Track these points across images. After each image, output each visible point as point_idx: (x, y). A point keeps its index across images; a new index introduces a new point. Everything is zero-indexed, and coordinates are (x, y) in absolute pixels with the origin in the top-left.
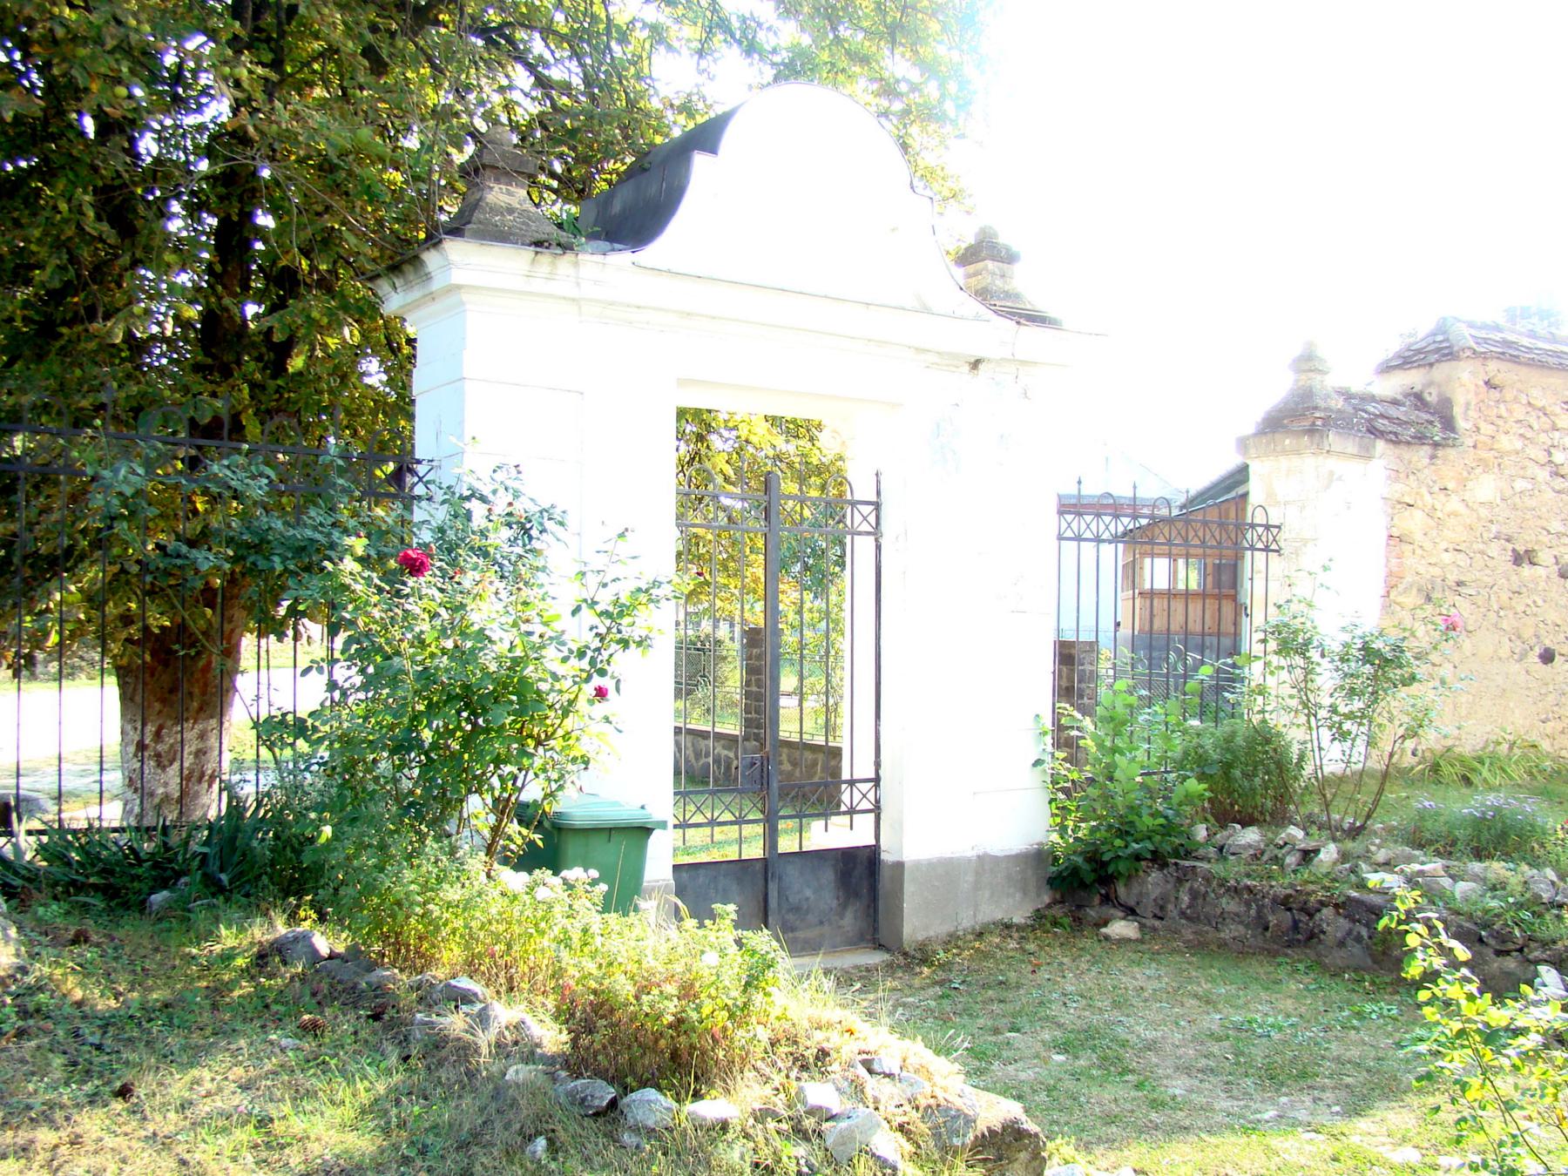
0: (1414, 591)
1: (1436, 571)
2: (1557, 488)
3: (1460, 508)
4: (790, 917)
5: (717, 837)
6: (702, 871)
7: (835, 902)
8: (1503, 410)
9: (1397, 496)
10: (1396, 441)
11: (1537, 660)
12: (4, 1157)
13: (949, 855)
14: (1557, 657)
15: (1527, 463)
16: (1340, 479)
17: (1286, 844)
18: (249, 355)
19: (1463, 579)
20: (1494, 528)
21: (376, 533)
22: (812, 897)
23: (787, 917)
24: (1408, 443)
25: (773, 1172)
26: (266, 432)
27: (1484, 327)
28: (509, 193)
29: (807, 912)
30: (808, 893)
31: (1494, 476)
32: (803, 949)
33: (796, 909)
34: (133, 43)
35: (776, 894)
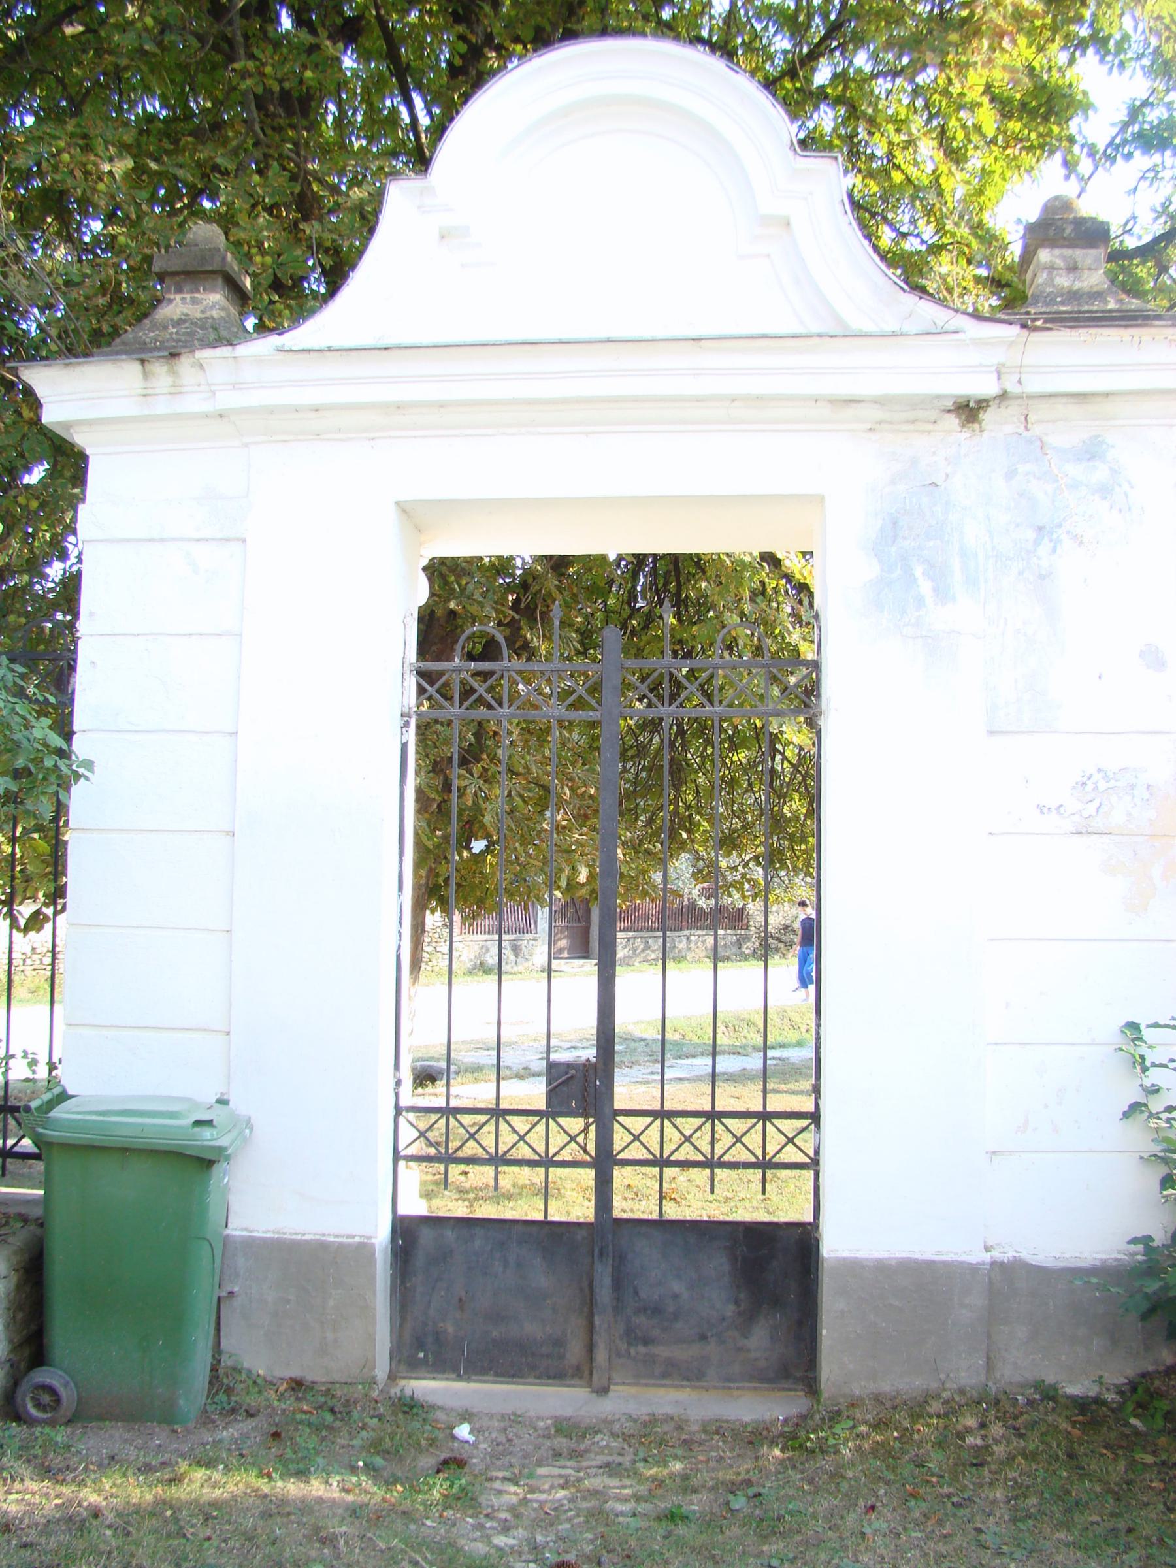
4: (641, 1320)
5: (505, 1183)
6: (479, 1231)
7: (730, 1310)
13: (929, 1256)
18: (736, 37)
22: (685, 1295)
23: (636, 1320)
28: (194, 301)
29: (676, 1316)
30: (677, 1287)
32: (665, 1375)
33: (656, 1310)
35: (607, 1281)
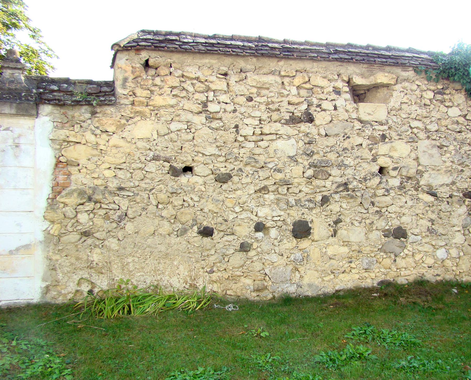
0: (75, 195)
1: (99, 182)
2: (447, 105)
3: (121, 143)
9: (62, 137)
10: (59, 104)
11: (196, 234)
12: (0, 314)
14: (216, 232)
15: (180, 112)
19: (123, 186)
20: (151, 154)
24: (70, 105)
25: (176, 378)
26: (235, 72)
27: (209, 37)
31: (151, 122)
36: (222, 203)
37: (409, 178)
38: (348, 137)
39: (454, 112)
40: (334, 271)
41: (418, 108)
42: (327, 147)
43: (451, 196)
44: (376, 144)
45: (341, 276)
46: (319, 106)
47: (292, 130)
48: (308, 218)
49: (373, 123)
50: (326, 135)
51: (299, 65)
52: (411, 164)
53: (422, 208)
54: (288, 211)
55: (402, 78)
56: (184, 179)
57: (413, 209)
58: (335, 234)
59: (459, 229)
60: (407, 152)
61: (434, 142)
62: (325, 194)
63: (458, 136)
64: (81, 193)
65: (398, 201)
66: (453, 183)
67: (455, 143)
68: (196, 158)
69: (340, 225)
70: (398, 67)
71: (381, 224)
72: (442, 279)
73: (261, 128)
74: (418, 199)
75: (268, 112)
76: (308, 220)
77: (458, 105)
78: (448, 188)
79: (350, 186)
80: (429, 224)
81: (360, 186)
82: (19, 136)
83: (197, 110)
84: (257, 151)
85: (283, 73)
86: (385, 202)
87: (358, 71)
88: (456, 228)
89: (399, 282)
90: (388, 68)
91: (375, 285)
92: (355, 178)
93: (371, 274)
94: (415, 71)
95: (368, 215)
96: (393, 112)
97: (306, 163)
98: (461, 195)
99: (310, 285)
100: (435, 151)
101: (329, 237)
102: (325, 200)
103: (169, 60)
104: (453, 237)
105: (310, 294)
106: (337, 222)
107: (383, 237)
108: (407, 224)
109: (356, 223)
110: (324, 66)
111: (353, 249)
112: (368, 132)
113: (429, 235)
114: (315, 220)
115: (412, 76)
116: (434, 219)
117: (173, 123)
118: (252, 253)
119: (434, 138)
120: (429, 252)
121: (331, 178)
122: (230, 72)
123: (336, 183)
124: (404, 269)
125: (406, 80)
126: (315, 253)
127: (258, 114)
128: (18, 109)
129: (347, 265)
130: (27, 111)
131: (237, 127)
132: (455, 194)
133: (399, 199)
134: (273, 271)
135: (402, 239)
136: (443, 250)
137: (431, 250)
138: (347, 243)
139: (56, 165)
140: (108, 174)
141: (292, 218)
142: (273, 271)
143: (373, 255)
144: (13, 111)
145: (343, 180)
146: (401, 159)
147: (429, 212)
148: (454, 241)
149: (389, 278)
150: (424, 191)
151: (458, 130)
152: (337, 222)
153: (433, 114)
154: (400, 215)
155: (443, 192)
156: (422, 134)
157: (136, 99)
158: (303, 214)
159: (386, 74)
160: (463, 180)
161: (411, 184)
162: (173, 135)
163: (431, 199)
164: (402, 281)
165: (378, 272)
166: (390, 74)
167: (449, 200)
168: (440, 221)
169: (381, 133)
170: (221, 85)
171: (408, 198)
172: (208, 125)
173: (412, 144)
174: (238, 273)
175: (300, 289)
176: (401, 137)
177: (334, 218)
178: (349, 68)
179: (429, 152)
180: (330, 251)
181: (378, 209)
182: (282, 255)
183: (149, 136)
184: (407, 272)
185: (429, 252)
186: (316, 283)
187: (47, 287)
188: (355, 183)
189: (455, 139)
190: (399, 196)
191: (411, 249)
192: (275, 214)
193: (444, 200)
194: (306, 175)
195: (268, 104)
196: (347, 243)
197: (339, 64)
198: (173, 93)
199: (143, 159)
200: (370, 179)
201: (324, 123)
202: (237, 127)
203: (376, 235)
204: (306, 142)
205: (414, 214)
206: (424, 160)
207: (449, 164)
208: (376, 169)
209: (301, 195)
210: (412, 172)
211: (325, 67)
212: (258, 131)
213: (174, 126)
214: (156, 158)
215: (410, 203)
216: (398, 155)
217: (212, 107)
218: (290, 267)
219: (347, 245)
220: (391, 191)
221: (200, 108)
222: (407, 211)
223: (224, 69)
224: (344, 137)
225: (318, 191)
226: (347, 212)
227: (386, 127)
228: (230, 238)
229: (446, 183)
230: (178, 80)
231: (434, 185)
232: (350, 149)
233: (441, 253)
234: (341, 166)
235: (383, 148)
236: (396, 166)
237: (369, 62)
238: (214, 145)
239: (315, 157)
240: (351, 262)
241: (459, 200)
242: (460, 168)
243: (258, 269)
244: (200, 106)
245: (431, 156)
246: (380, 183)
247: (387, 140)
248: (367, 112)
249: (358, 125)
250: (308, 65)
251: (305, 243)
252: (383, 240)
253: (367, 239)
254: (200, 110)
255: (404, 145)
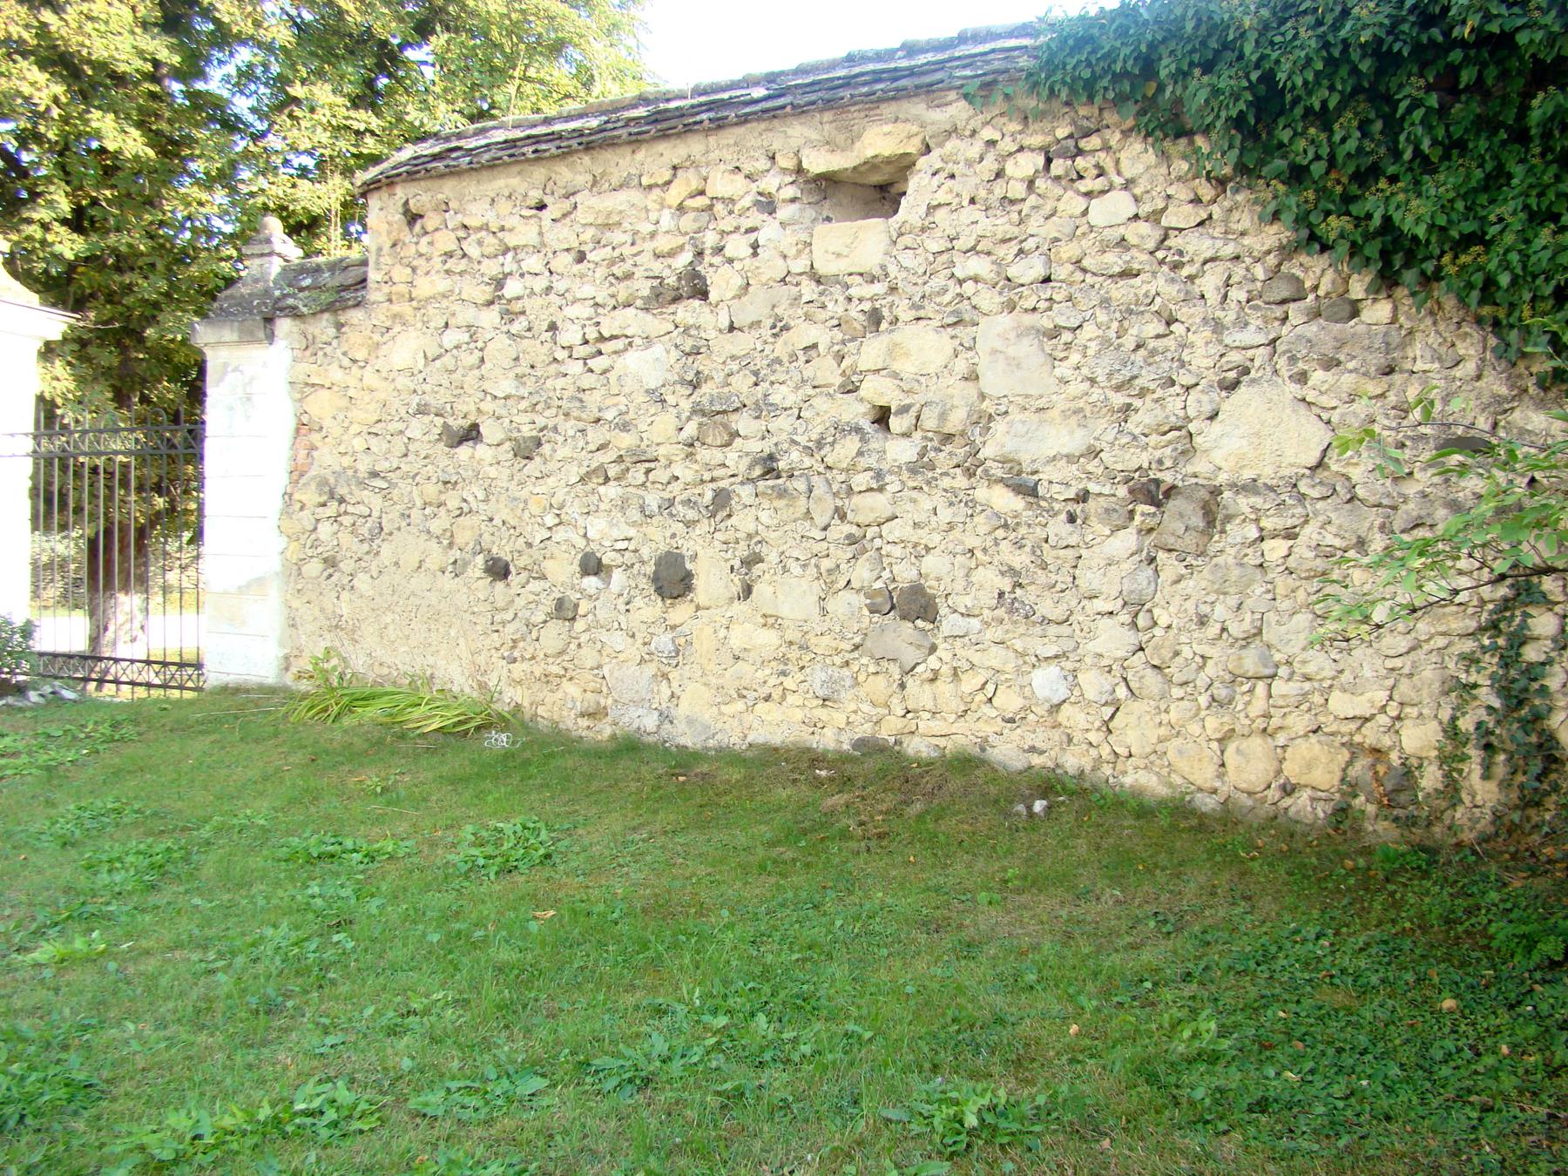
0: (313, 486)
1: (347, 461)
8: (423, 248)
9: (302, 378)
16: (236, 369)
17: (969, 584)
21: (142, 395)
34: (237, 138)
36: (522, 505)
37: (948, 438)
38: (786, 328)
39: (1113, 209)
40: (745, 692)
41: (979, 216)
42: (733, 358)
43: (1083, 497)
44: (853, 339)
45: (762, 707)
46: (719, 250)
47: (656, 322)
48: (687, 548)
49: (849, 280)
50: (732, 328)
51: (673, 151)
52: (956, 392)
53: (982, 530)
54: (644, 529)
55: (935, 128)
56: (464, 451)
57: (956, 533)
58: (748, 591)
59: (1108, 607)
60: (940, 360)
61: (1029, 319)
62: (721, 484)
63: (1121, 292)
64: (322, 482)
65: (909, 506)
66: (1094, 453)
67: (1102, 317)
68: (482, 406)
69: (758, 569)
70: (916, 100)
71: (862, 573)
72: (1050, 764)
73: (598, 324)
74: (971, 503)
75: (612, 284)
76: (684, 551)
77: (1128, 185)
78: (1074, 467)
79: (782, 465)
80: (1006, 584)
81: (808, 462)
82: (252, 379)
83: (481, 299)
84: (588, 381)
85: (645, 181)
86: (872, 510)
87: (814, 136)
88: (1101, 605)
89: (910, 751)
90: (888, 110)
91: (846, 747)
92: (794, 442)
93: (835, 715)
94: (966, 96)
95: (825, 545)
96: (906, 240)
97: (686, 405)
98: (1122, 491)
99: (690, 721)
100: (1028, 349)
101: (731, 600)
102: (722, 499)
103: (440, 196)
104: (1091, 635)
105: (690, 744)
106: (752, 561)
107: (866, 612)
108: (939, 579)
109: (795, 568)
110: (731, 142)
111: (788, 637)
112: (836, 308)
113: (1006, 617)
114: (701, 553)
115: (965, 116)
116: (1018, 567)
117: (448, 331)
118: (580, 625)
119: (1029, 304)
120: (1005, 672)
121: (738, 442)
122: (548, 200)
123: (747, 454)
124: (927, 715)
125: (952, 132)
126: (703, 636)
127: (587, 291)
128: (241, 331)
129: (773, 681)
130: (252, 333)
131: (553, 327)
132: (1093, 488)
133: (914, 501)
134: (616, 674)
135: (919, 623)
136: (1053, 670)
137: (1010, 667)
138: (771, 621)
139: (297, 431)
140: (359, 443)
141: (654, 546)
142: (616, 674)
143: (838, 660)
144: (235, 337)
145: (767, 447)
146: (923, 379)
147: (1004, 545)
148: (1093, 647)
149: (886, 733)
150: (992, 481)
151: (1117, 270)
152: (752, 561)
153: (1033, 225)
154: (921, 551)
155: (1058, 482)
156: (988, 296)
157: (394, 289)
158: (674, 536)
159: (887, 128)
160: (1124, 440)
161: (950, 454)
162: (448, 360)
163: (1015, 503)
164: (918, 747)
165: (855, 712)
166: (900, 126)
167: (1078, 509)
168: (1042, 577)
169: (867, 306)
170: (525, 233)
171: (938, 500)
172: (505, 329)
173: (958, 330)
174: (556, 669)
175: (667, 726)
176: (922, 313)
177: (742, 551)
178: (790, 131)
179: (1011, 351)
180: (737, 639)
181: (854, 530)
182: (633, 636)
183: (410, 363)
184: (938, 726)
185: (1005, 672)
186: (707, 716)
187: (287, 658)
188: (795, 455)
189: (1105, 302)
190: (914, 494)
191: (947, 656)
192: (616, 534)
193: (1056, 506)
194: (684, 435)
195: (612, 263)
196: (771, 621)
197: (763, 126)
198: (447, 266)
199: (403, 414)
200: (833, 444)
201: (729, 295)
202: (553, 327)
203: (846, 605)
204: (687, 350)
205: (959, 549)
206: (994, 381)
207: (1077, 388)
208: (855, 411)
209: (676, 487)
210: (956, 420)
211: (736, 144)
212: (592, 334)
213: (451, 338)
214: (422, 410)
215: (945, 515)
216: (913, 370)
217: (512, 288)
218: (650, 669)
219: (772, 626)
220: (888, 479)
221: (486, 292)
222: (937, 538)
223: (535, 195)
224: (774, 327)
225: (707, 476)
226: (773, 535)
227: (879, 288)
228: (535, 586)
229: (1065, 451)
230: (453, 236)
231: (1025, 458)
232: (785, 359)
233: (1047, 682)
234: (763, 409)
235: (871, 352)
236: (907, 401)
237: (829, 104)
238: (512, 374)
239: (706, 388)
240: (784, 673)
241: (1107, 510)
242: (1119, 399)
243: (589, 664)
244: (489, 289)
245: (1015, 364)
246: (860, 453)
247: (884, 325)
248: (831, 249)
249: (809, 290)
250: (694, 146)
251: (680, 612)
252: (867, 620)
253: (824, 612)
254: (489, 297)
255: (932, 336)
